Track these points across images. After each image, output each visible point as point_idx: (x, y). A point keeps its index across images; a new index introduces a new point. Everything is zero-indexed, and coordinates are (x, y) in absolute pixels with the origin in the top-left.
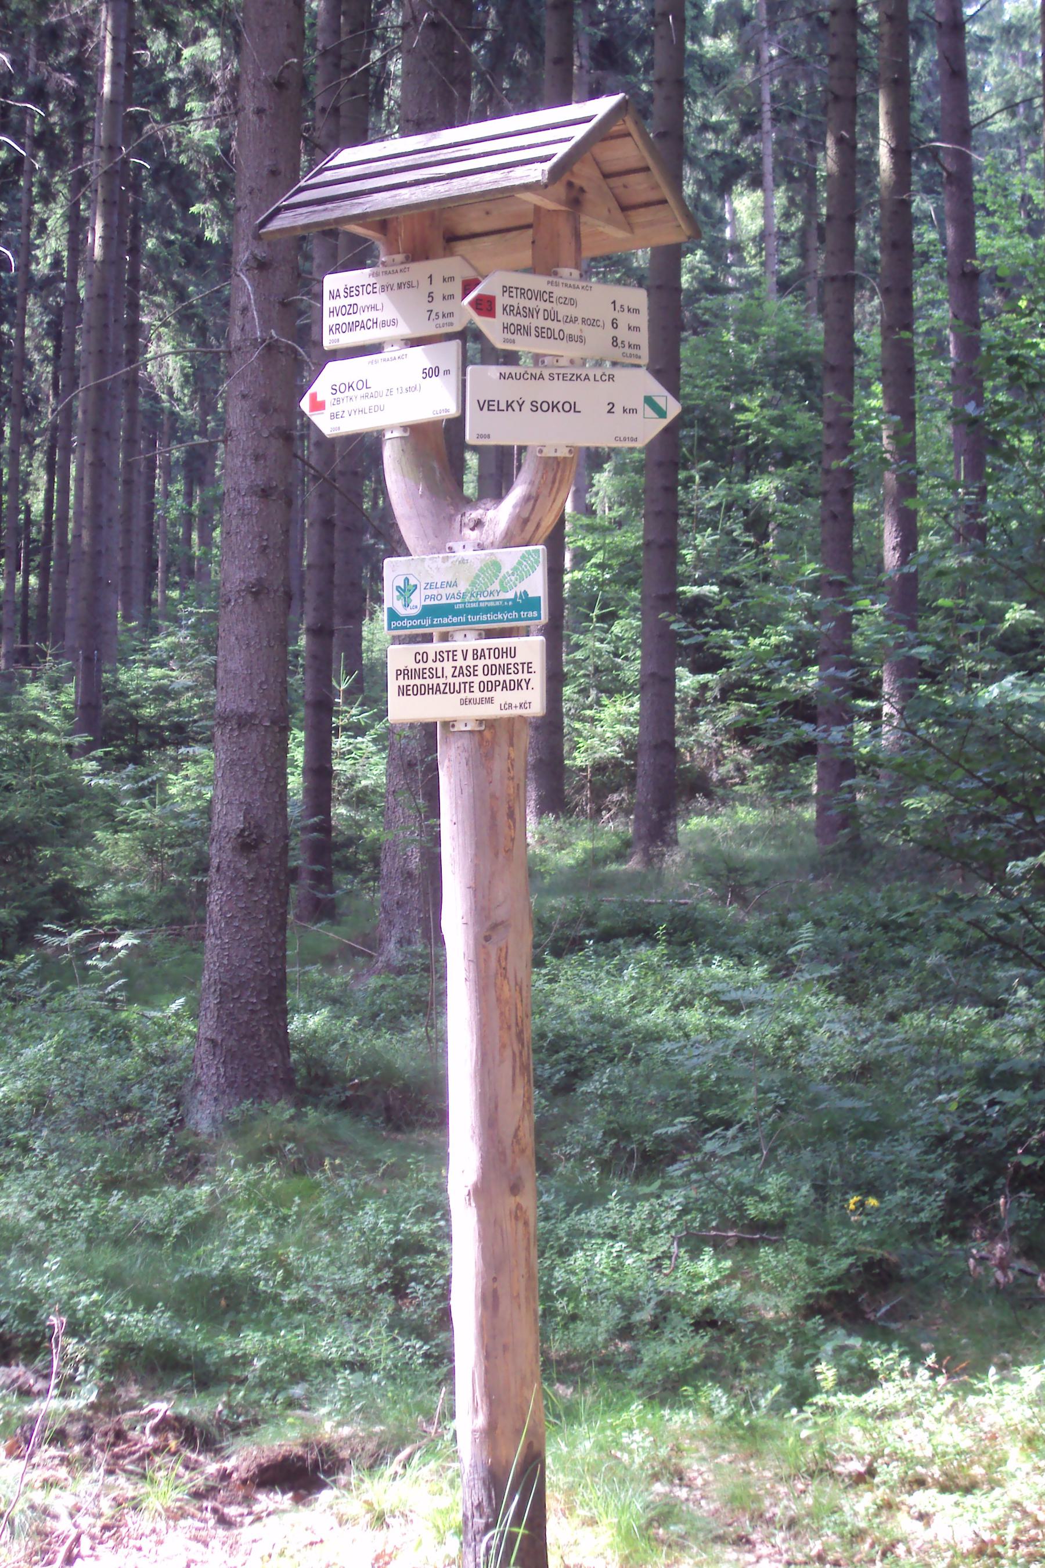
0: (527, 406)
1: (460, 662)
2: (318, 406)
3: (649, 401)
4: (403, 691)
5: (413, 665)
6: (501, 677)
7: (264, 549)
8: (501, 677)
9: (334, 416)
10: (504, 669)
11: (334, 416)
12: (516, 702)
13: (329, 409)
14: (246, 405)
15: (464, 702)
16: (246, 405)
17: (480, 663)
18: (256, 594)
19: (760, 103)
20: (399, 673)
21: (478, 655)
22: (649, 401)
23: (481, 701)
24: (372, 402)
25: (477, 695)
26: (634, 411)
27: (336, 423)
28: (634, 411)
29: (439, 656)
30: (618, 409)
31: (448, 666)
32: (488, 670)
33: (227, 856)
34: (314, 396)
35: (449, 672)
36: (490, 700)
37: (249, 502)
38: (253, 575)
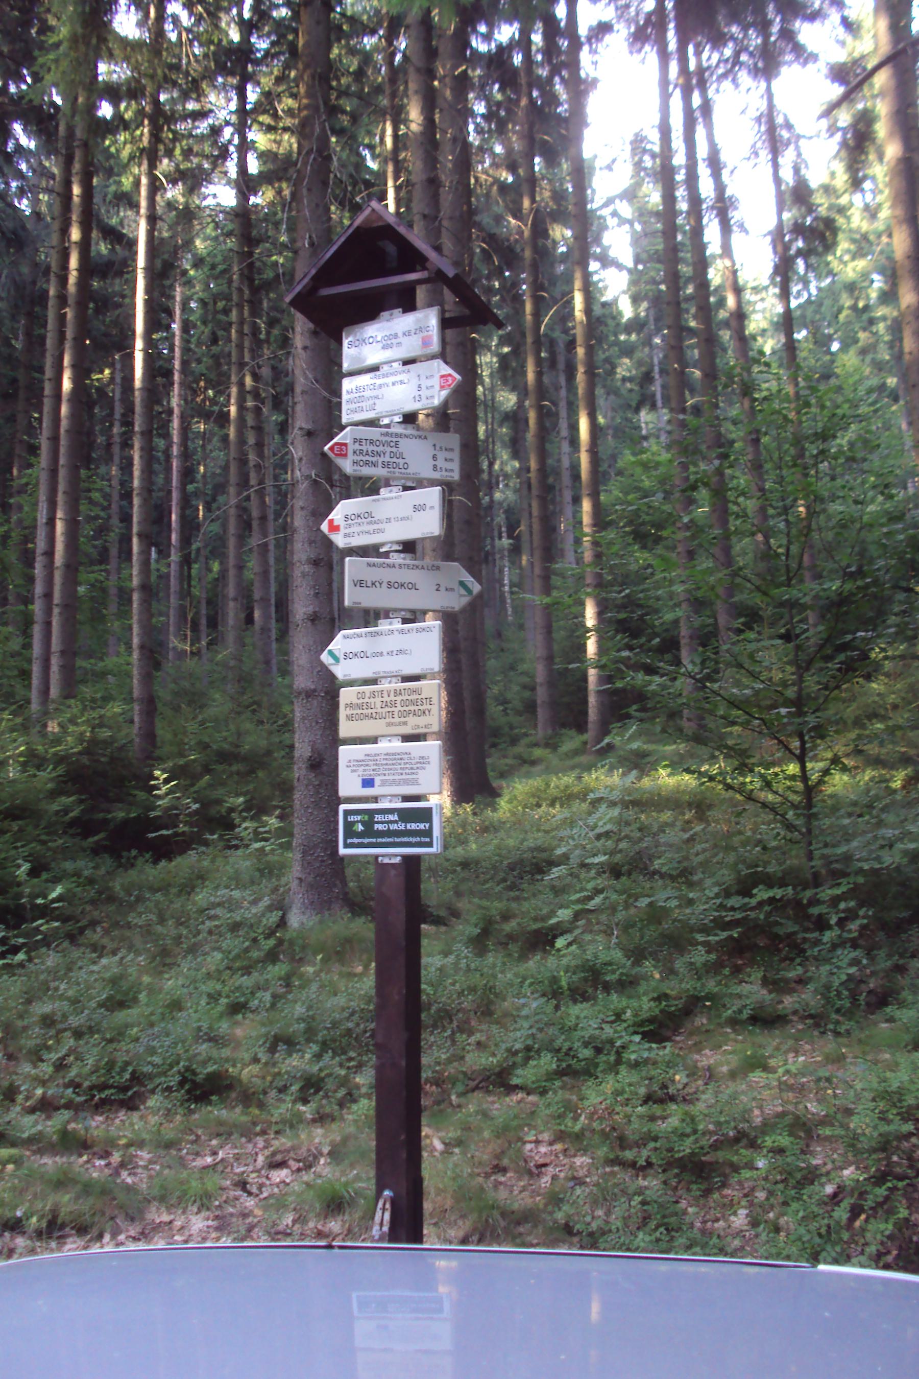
0: (385, 585)
1: (386, 698)
2: (334, 528)
3: (337, 660)
4: (349, 718)
5: (355, 701)
6: (412, 708)
7: (316, 595)
8: (412, 708)
9: (346, 535)
10: (412, 702)
11: (346, 535)
12: (422, 724)
13: (343, 531)
14: (304, 513)
15: (389, 724)
16: (304, 513)
17: (399, 698)
18: (313, 621)
19: (652, 366)
20: (347, 705)
21: (397, 693)
22: (462, 584)
23: (400, 724)
24: (376, 527)
25: (397, 720)
26: (452, 590)
27: (348, 540)
28: (452, 590)
29: (373, 694)
30: (442, 589)
31: (378, 700)
32: (405, 703)
33: (304, 772)
34: (331, 521)
35: (379, 705)
36: (405, 723)
37: (307, 568)
38: (311, 609)
